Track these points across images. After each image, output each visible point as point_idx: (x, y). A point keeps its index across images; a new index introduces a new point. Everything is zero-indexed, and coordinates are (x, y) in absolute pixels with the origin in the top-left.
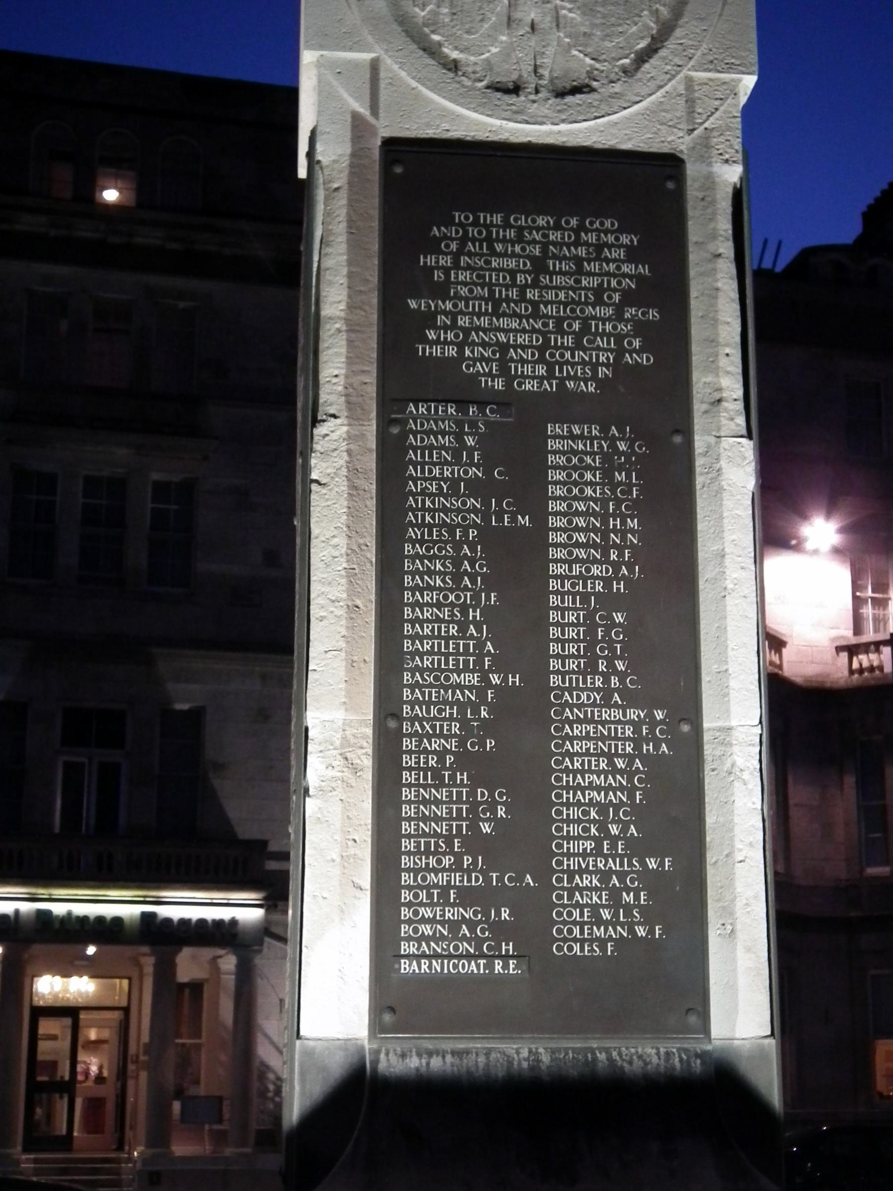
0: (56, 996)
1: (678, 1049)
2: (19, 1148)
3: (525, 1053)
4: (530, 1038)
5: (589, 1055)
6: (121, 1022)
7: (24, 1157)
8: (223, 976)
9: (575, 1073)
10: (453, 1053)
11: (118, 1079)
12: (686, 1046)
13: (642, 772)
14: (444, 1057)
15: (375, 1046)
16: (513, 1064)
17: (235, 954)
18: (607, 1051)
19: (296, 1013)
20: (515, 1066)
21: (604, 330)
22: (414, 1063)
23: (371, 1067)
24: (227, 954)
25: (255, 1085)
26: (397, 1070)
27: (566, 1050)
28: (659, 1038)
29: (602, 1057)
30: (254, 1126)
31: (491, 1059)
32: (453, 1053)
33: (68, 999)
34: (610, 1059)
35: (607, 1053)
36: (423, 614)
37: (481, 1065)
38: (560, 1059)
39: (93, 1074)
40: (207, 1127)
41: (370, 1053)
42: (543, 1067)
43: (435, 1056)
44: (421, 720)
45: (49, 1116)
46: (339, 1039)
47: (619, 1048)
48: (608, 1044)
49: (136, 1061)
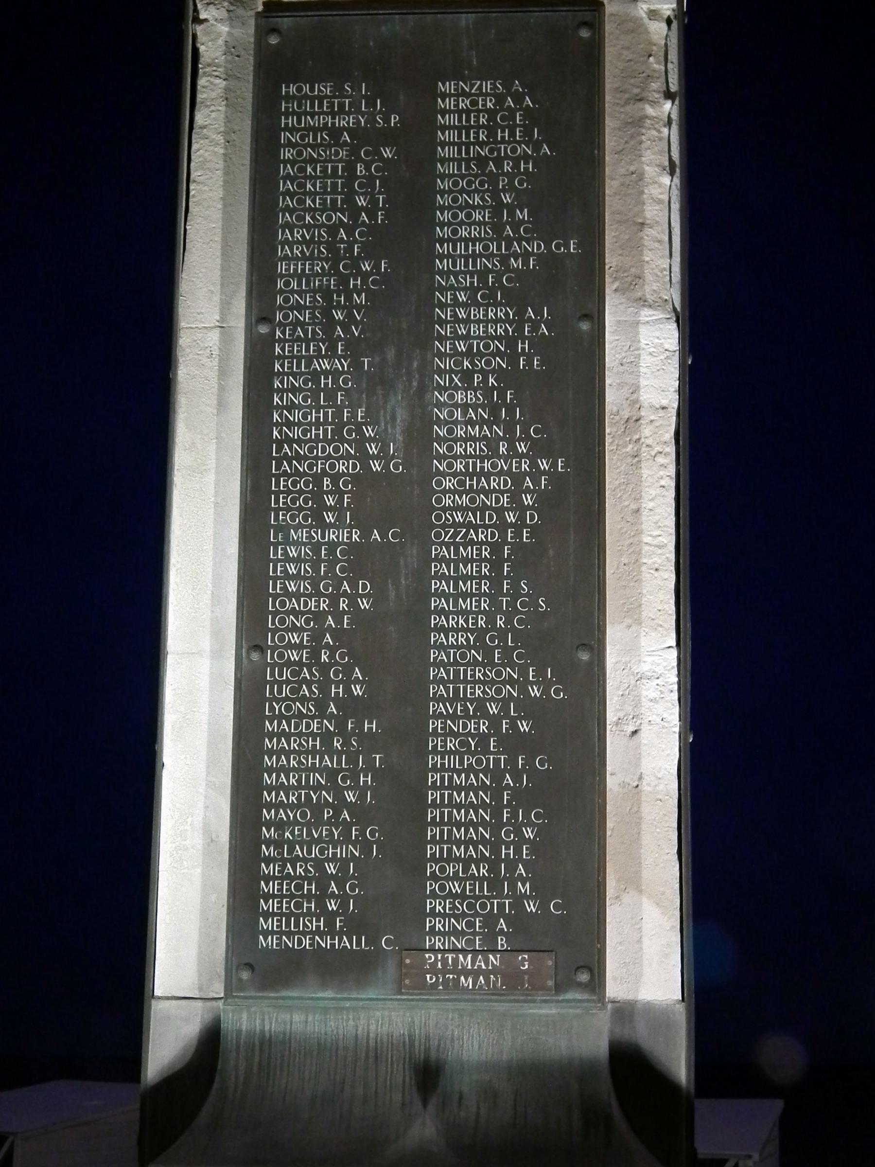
21: (482, 468)
36: (289, 745)
44: (288, 736)
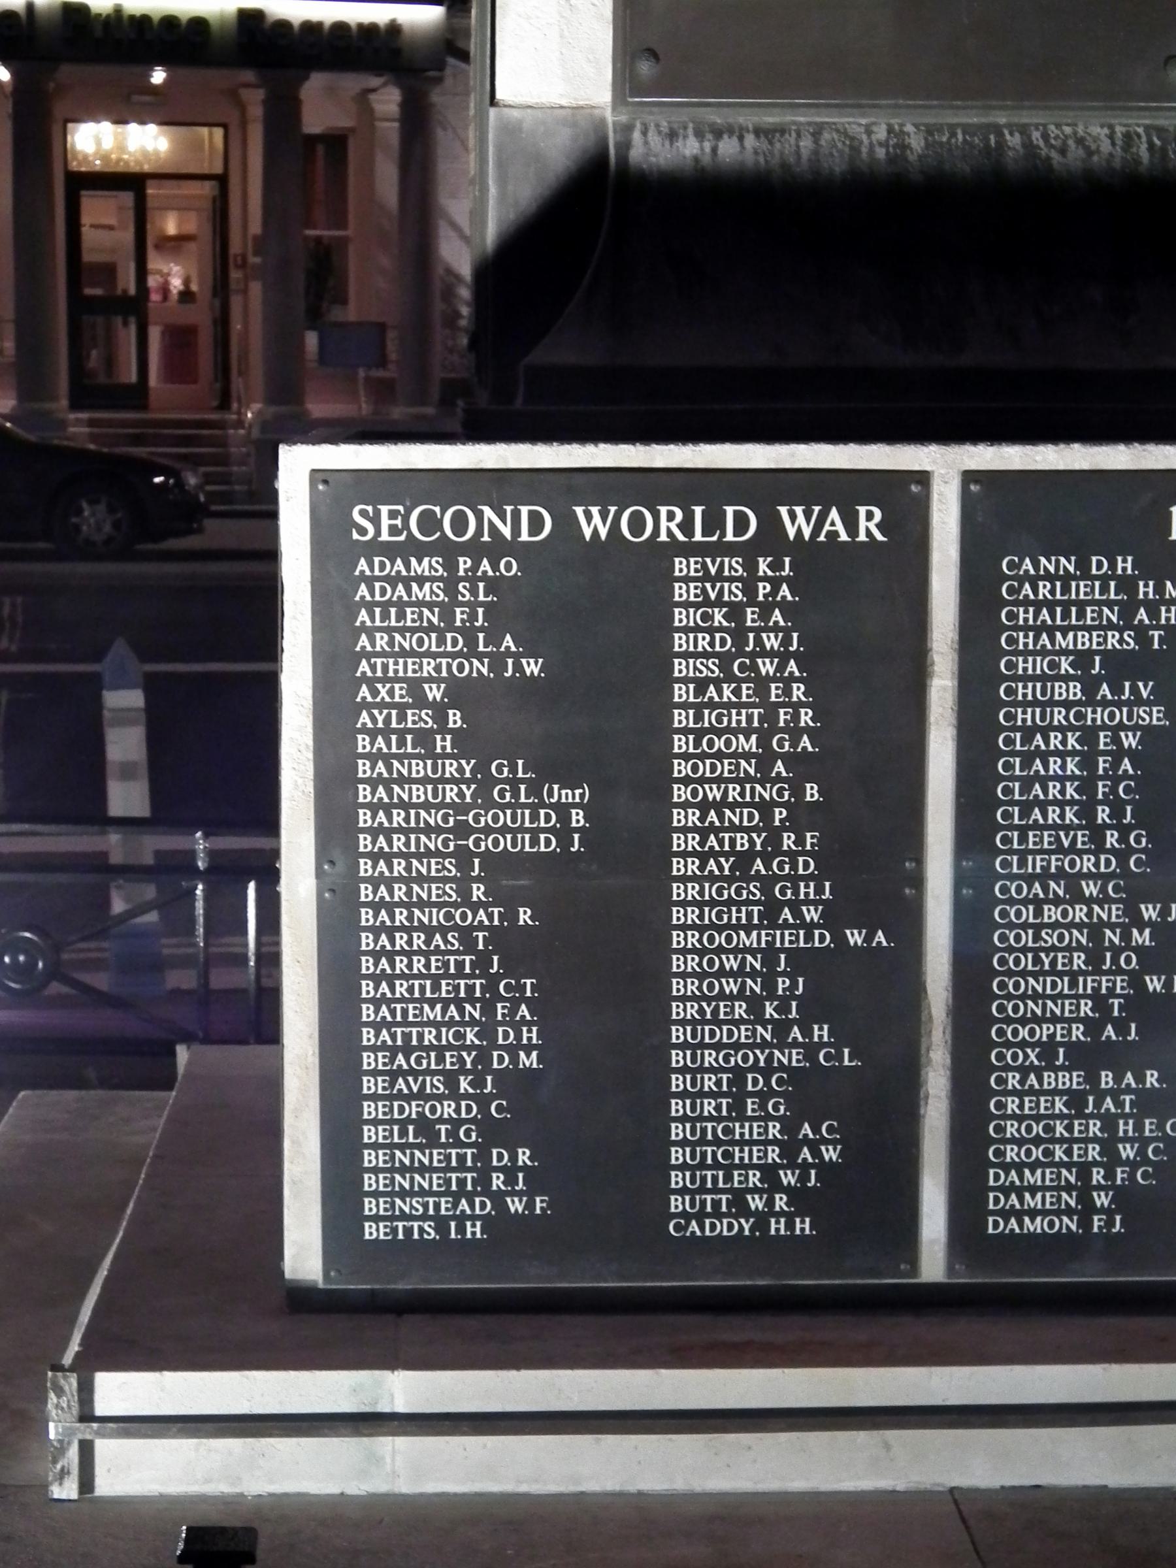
0: (105, 158)
1: (1147, 128)
2: (64, 402)
3: (881, 133)
4: (888, 106)
5: (992, 137)
6: (214, 200)
7: (72, 416)
8: (378, 124)
9: (967, 169)
10: (758, 132)
11: (215, 295)
12: (1161, 122)
13: (1131, 778)
14: (741, 138)
15: (623, 118)
16: (860, 152)
17: (399, 84)
18: (1024, 130)
19: (488, 61)
20: (864, 155)
22: (690, 147)
23: (617, 154)
24: (385, 85)
25: (438, 306)
26: (662, 161)
27: (952, 130)
28: (1113, 109)
29: (1014, 140)
30: (438, 374)
31: (823, 143)
32: (758, 132)
33: (127, 163)
34: (1028, 145)
35: (1021, 133)
37: (805, 153)
38: (941, 144)
39: (175, 291)
40: (362, 373)
41: (615, 131)
42: (912, 158)
43: (725, 136)
45: (110, 362)
46: (562, 107)
47: (1045, 126)
48: (1025, 118)
49: (243, 265)
